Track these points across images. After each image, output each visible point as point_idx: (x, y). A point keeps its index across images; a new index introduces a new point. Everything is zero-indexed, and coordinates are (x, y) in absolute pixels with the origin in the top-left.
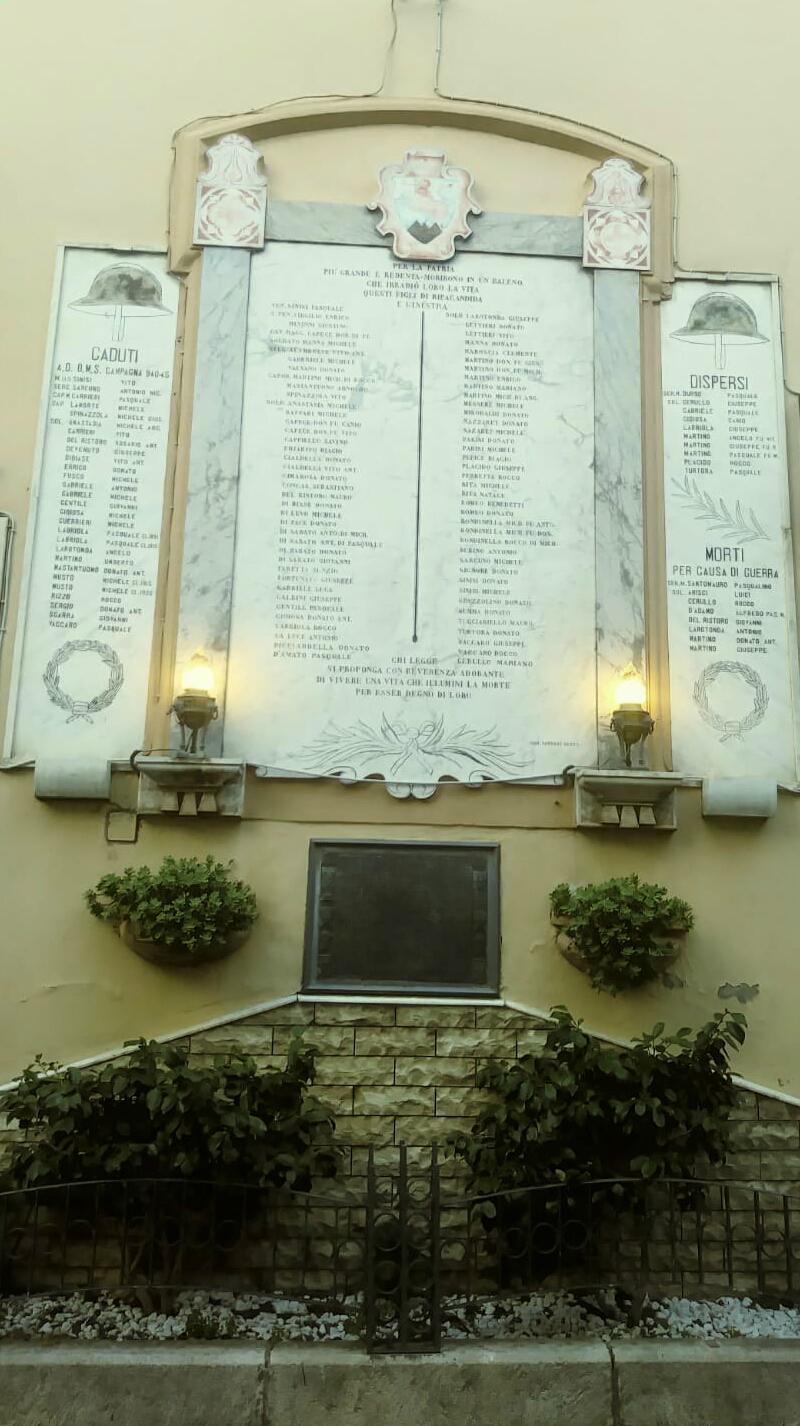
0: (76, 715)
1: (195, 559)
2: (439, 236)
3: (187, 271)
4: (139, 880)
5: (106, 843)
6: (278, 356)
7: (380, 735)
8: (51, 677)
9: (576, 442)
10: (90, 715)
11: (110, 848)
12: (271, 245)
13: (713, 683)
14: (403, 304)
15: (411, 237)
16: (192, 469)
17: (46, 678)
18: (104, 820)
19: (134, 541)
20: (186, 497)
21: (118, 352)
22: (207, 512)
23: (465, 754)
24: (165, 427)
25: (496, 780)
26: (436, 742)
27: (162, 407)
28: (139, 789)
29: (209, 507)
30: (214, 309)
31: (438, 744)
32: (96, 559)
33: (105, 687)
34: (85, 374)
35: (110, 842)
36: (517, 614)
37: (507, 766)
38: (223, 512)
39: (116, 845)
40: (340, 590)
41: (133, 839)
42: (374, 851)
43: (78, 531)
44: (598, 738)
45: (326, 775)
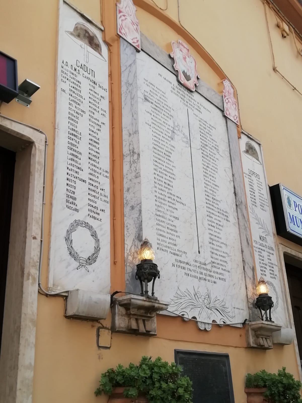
0: (81, 265)
1: (128, 190)
2: (190, 81)
3: (112, 44)
4: (254, 380)
5: (97, 348)
6: (147, 103)
7: (193, 296)
8: (68, 239)
9: (229, 181)
10: (87, 266)
11: (99, 352)
12: (141, 52)
13: (77, 252)
14: (182, 102)
15: (98, 37)
16: (124, 143)
17: (66, 240)
18: (95, 332)
19: (100, 171)
20: (122, 156)
21: (87, 68)
22: (131, 167)
23: (218, 310)
24: (107, 115)
25: (227, 324)
26: (210, 303)
27: (105, 105)
28: (117, 315)
29: (131, 165)
30: (126, 69)
31: (211, 304)
32: (84, 175)
33: (93, 251)
34: (74, 72)
35: (99, 347)
36: (224, 249)
37: (229, 317)
38: (136, 170)
39: (102, 349)
40: (176, 222)
41: (100, 345)
42: (194, 357)
43: (77, 157)
44: (249, 308)
45: (180, 315)
